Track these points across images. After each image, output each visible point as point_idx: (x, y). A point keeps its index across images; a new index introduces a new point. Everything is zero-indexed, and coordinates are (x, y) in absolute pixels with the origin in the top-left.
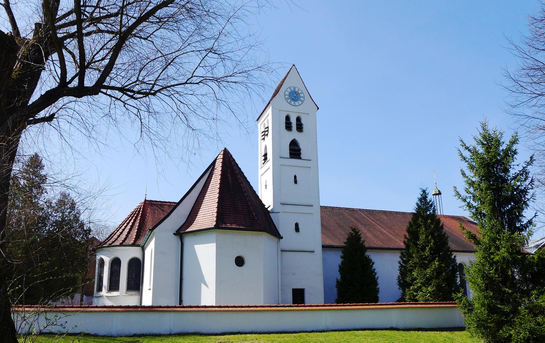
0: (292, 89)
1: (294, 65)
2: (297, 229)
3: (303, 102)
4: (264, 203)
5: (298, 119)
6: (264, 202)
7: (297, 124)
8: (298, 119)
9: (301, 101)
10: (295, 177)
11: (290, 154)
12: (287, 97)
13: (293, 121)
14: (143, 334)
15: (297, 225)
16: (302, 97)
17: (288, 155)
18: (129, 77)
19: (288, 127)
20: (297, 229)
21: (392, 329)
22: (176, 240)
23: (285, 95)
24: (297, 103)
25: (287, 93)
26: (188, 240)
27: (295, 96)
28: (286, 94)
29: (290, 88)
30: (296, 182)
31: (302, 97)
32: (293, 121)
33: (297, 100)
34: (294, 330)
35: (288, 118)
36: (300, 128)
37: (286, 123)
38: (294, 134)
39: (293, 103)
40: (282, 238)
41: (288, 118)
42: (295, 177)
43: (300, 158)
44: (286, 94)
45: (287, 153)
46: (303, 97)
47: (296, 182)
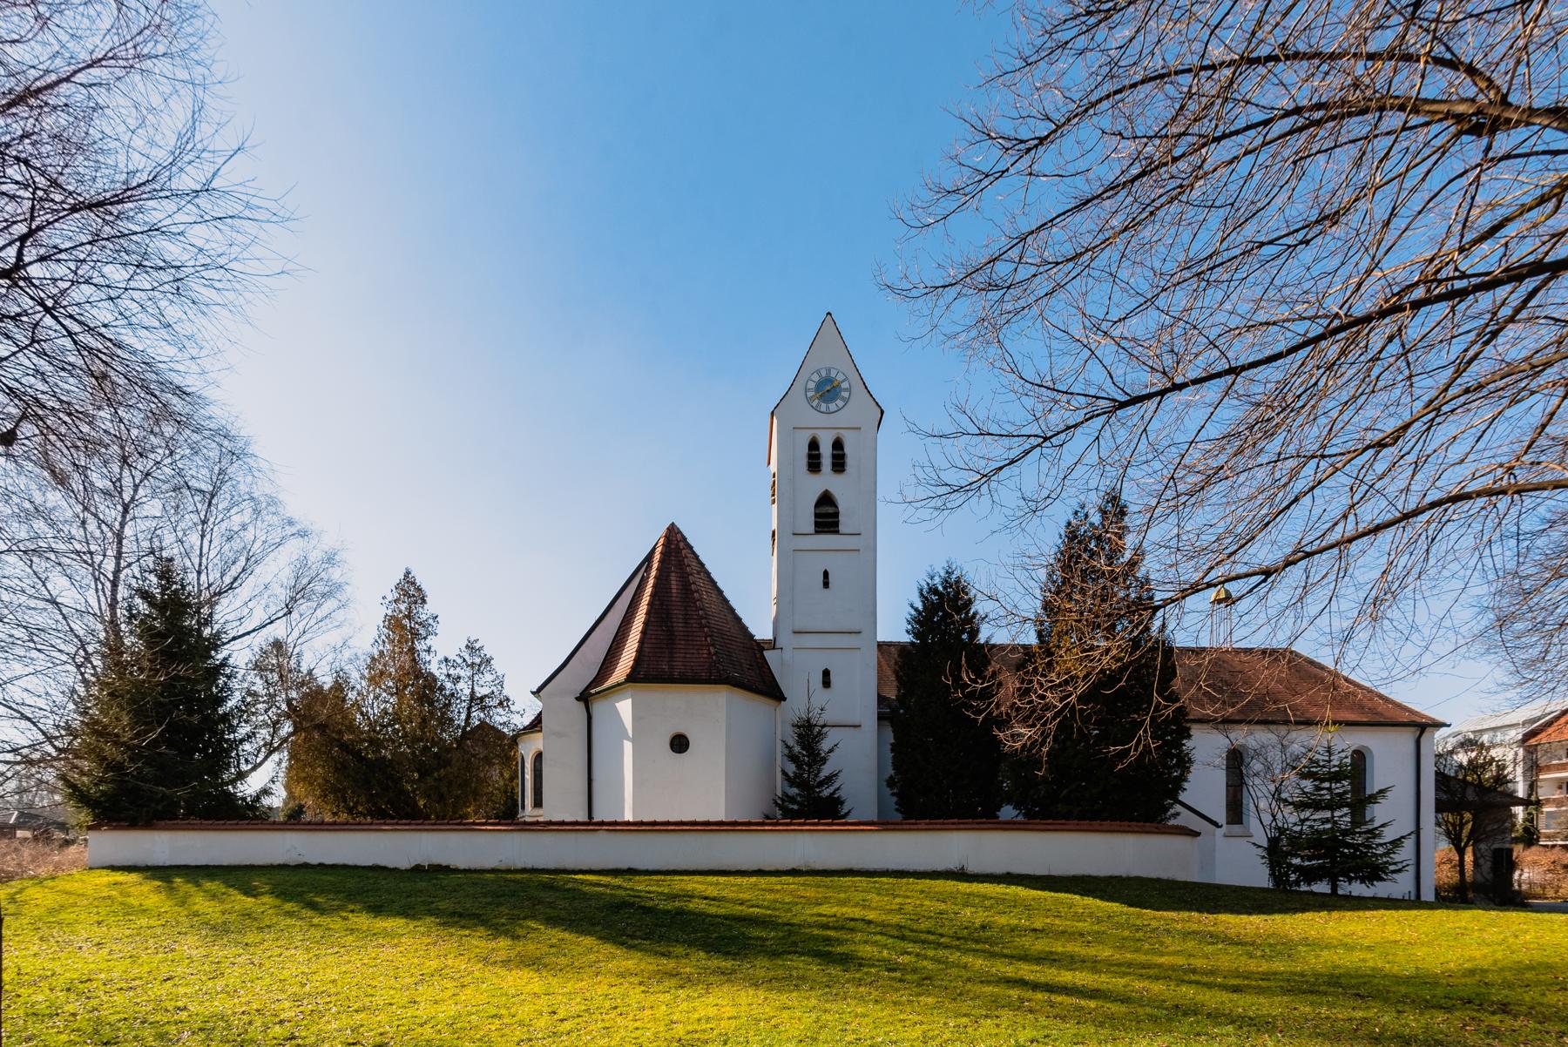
0: (824, 374)
1: (829, 314)
2: (827, 683)
3: (846, 401)
4: (753, 633)
5: (838, 445)
6: (752, 630)
7: (834, 456)
8: (838, 445)
9: (843, 399)
10: (826, 574)
11: (817, 524)
12: (810, 394)
13: (826, 451)
14: (887, 870)
15: (826, 673)
16: (846, 390)
17: (812, 529)
18: (1333, 253)
19: (814, 465)
20: (827, 683)
21: (794, 872)
22: (581, 705)
23: (806, 390)
24: (832, 407)
25: (812, 385)
26: (598, 708)
27: (828, 391)
28: (809, 387)
29: (818, 372)
30: (826, 585)
31: (846, 390)
32: (826, 451)
33: (833, 400)
34: (739, 868)
35: (814, 445)
36: (839, 464)
37: (810, 456)
38: (827, 480)
39: (823, 407)
40: (785, 699)
41: (814, 445)
42: (826, 574)
43: (837, 532)
44: (809, 387)
45: (807, 521)
46: (849, 390)
47: (826, 585)
